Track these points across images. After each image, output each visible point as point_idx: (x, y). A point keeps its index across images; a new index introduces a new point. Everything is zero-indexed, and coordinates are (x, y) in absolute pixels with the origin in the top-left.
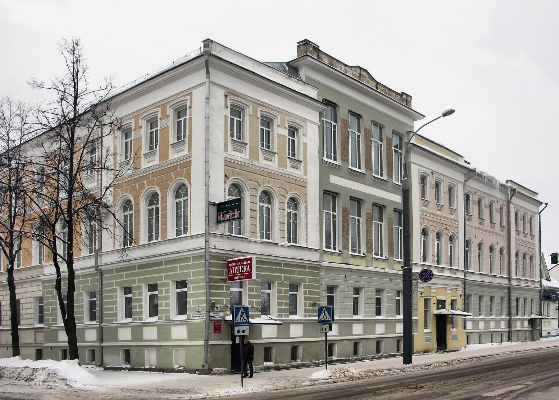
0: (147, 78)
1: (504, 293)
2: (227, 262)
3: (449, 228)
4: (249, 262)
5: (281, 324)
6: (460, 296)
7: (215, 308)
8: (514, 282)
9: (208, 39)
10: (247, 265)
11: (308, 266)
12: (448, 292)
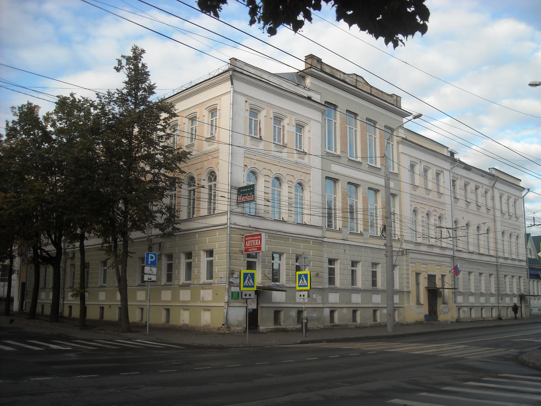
3: (437, 210)
4: (260, 237)
6: (450, 272)
9: (233, 58)
10: (258, 239)
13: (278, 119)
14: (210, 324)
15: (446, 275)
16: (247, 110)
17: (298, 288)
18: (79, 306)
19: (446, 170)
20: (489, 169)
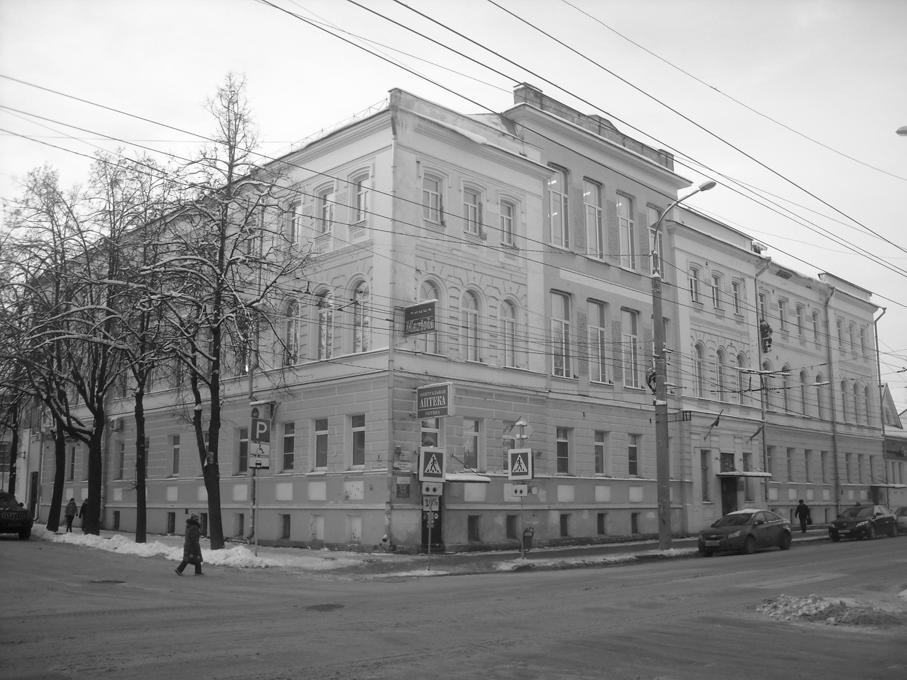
0: (321, 136)
1: (827, 446)
2: (417, 391)
3: (734, 344)
4: (445, 391)
5: (488, 482)
7: (401, 457)
8: (840, 429)
9: (396, 89)
11: (530, 398)
12: (737, 441)
13: (473, 193)
14: (360, 540)
15: (794, 448)
16: (420, 177)
17: (511, 478)
18: (136, 511)
19: (749, 277)
20: (819, 275)
